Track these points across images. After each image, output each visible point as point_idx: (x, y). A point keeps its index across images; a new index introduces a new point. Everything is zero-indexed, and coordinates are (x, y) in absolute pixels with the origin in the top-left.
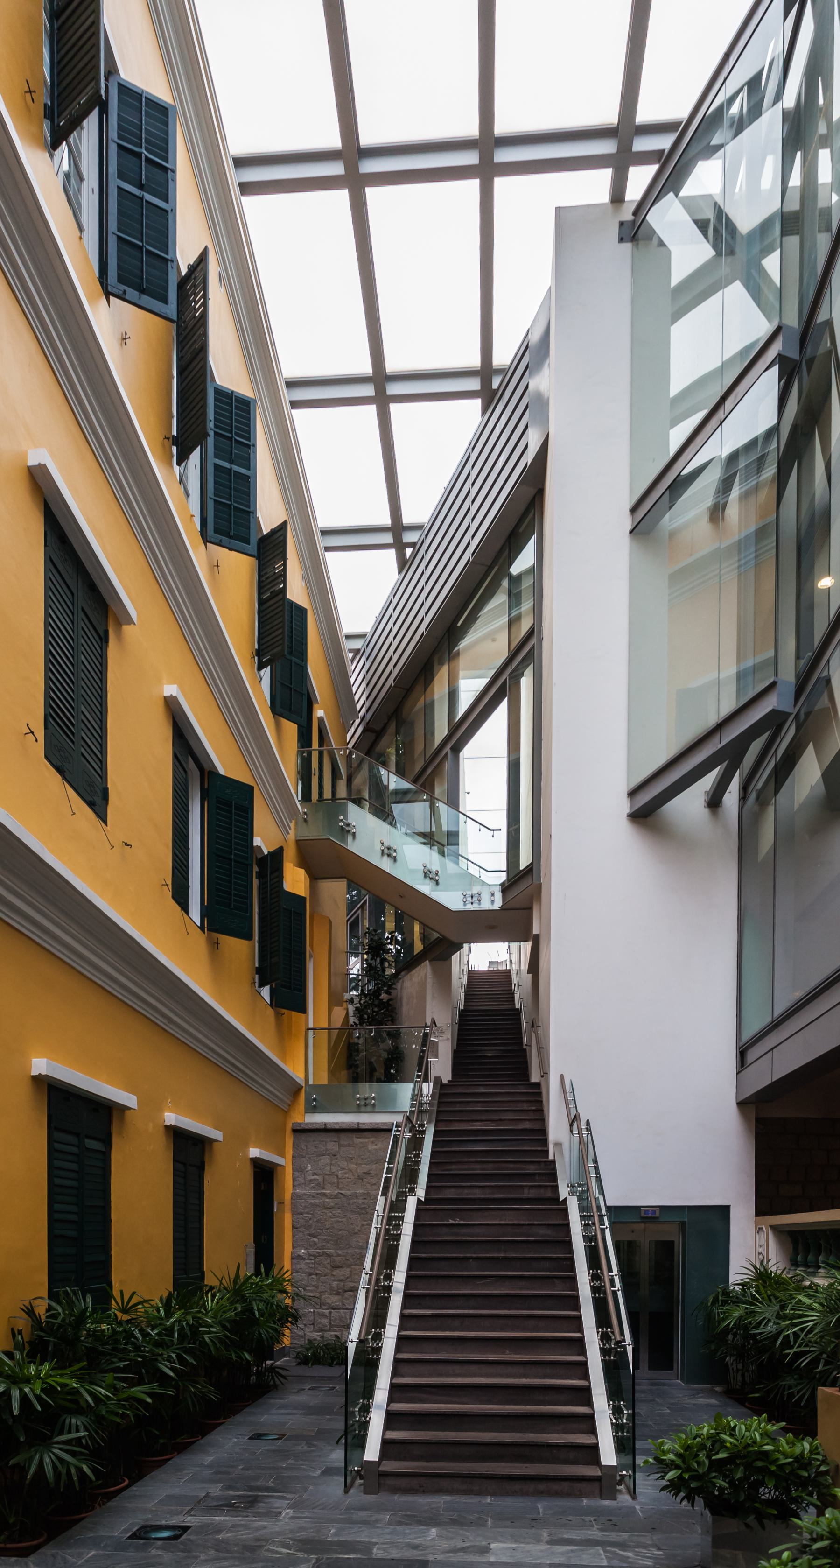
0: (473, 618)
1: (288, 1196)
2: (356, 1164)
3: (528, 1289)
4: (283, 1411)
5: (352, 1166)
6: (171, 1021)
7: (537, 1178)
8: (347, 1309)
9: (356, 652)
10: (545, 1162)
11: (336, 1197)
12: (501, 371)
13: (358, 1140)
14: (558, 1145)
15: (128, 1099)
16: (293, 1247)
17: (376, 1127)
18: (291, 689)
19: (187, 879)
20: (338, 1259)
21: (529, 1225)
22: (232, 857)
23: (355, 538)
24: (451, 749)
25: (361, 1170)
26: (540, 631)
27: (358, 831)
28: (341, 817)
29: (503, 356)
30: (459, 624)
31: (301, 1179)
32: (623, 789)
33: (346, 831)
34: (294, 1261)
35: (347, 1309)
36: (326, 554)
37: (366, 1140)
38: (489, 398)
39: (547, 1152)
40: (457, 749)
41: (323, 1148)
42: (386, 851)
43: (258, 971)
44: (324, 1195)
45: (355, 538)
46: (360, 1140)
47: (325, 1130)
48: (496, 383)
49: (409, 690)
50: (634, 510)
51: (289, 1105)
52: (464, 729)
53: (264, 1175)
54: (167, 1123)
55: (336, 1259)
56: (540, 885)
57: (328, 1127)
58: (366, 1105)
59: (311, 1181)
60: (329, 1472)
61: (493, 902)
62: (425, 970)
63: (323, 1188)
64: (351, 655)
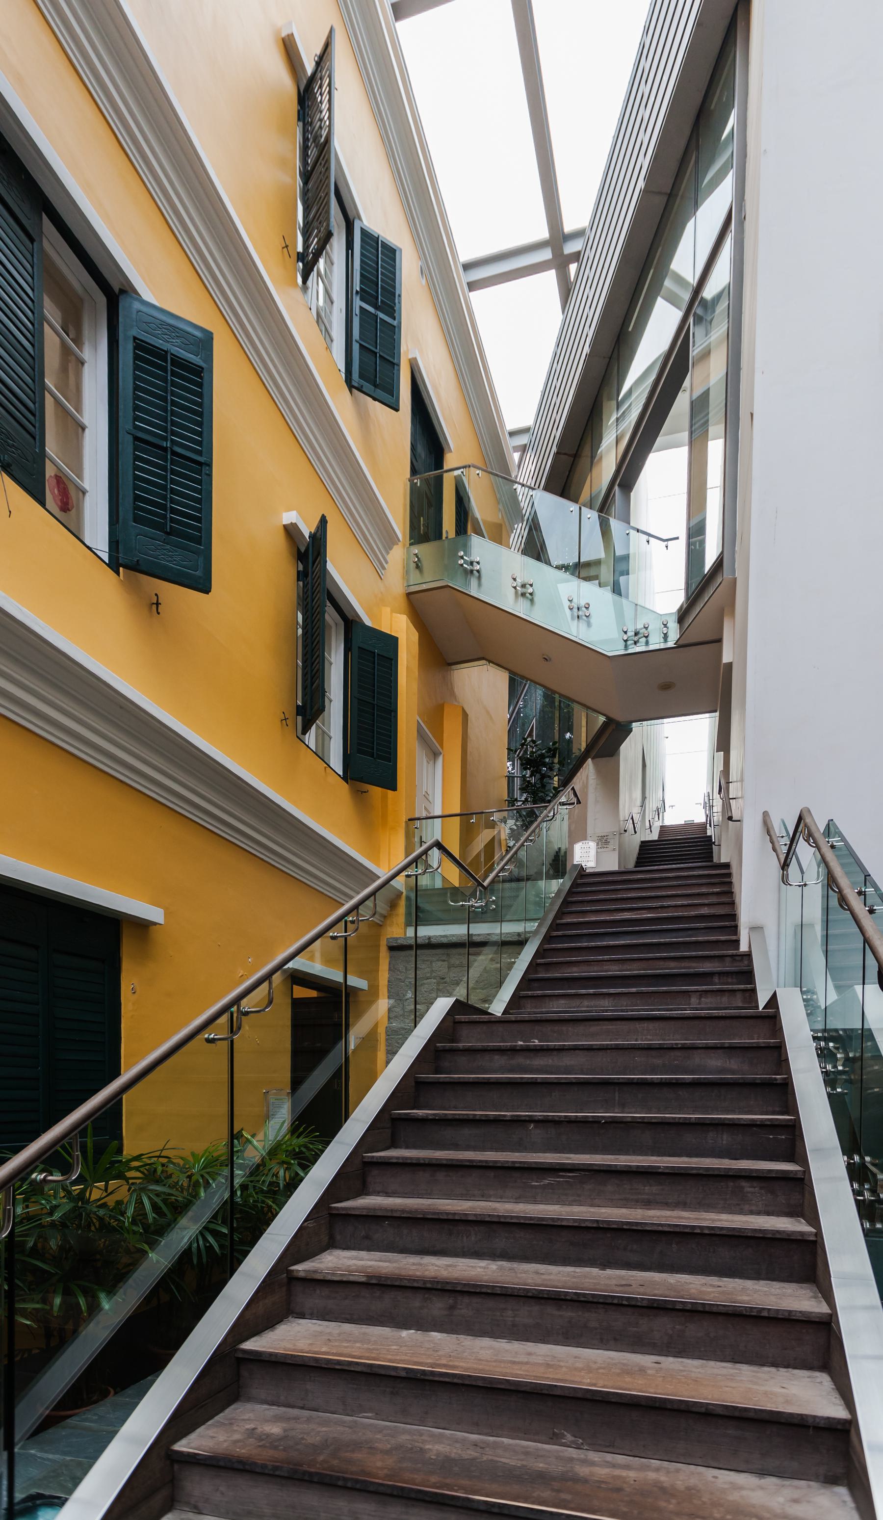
9: (524, 449)
10: (732, 956)
14: (756, 929)
21: (684, 1048)
23: (503, 267)
27: (485, 568)
28: (462, 553)
30: (630, 329)
33: (471, 572)
36: (472, 294)
39: (737, 942)
45: (503, 267)
49: (576, 456)
51: (385, 917)
56: (734, 581)
57: (433, 941)
61: (666, 637)
64: (516, 456)
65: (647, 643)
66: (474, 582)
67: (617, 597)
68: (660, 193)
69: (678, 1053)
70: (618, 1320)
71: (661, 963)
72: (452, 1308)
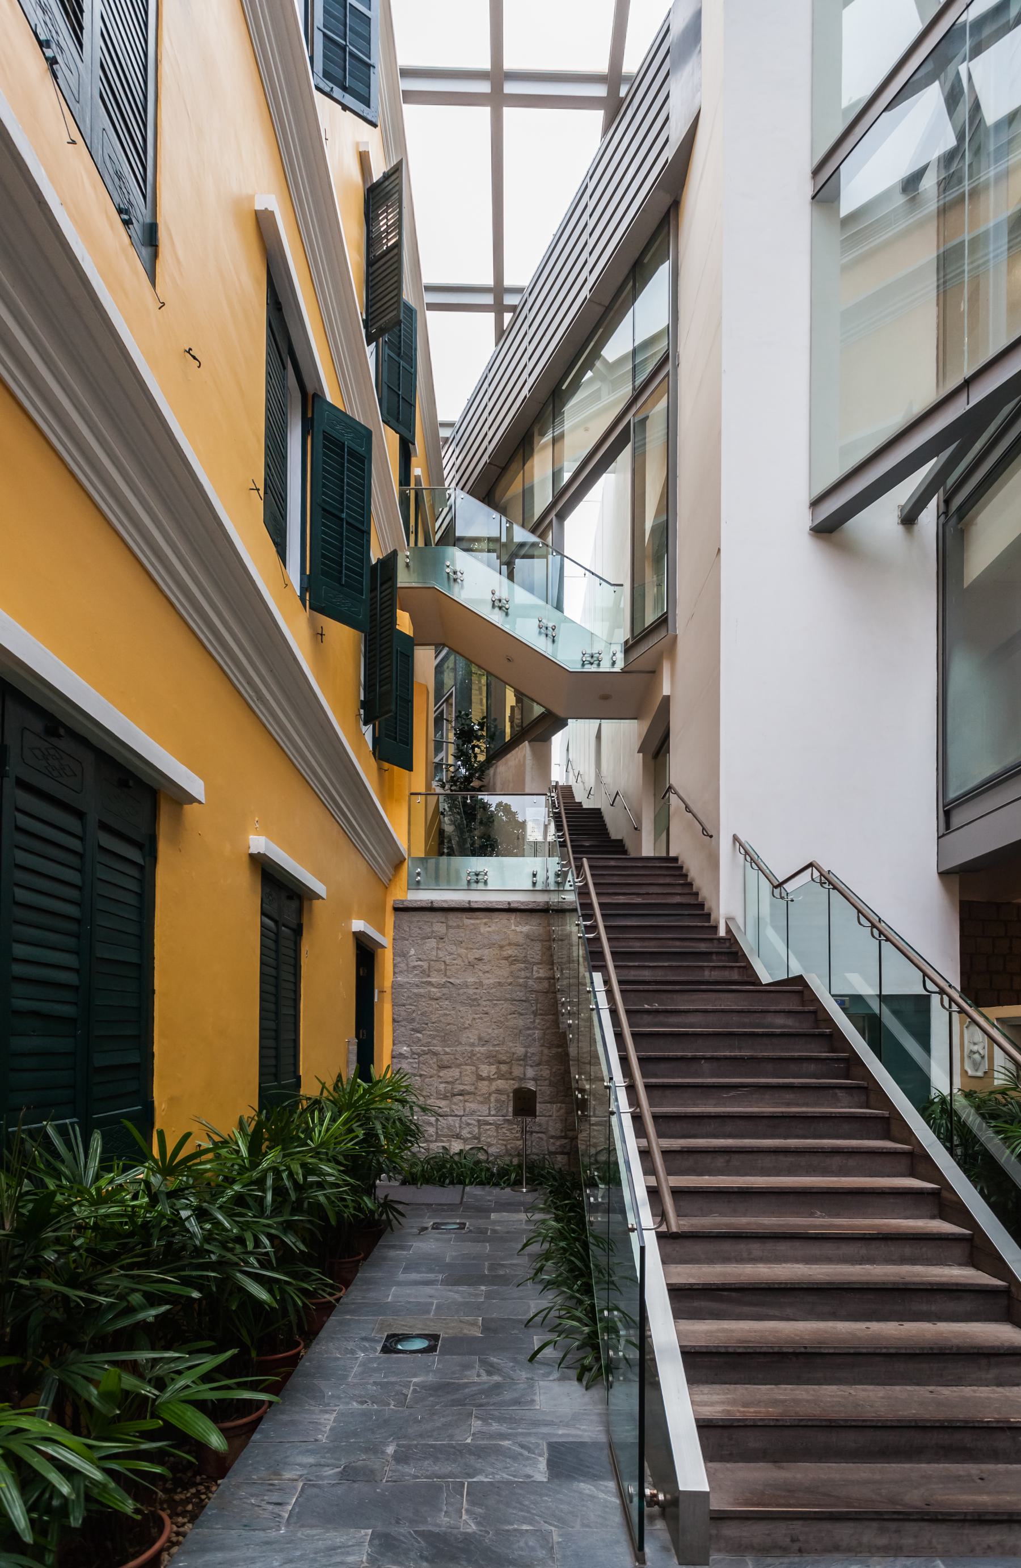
0: (575, 386)
1: (387, 984)
2: (467, 949)
3: (798, 1105)
4: (414, 1276)
5: (463, 951)
6: (261, 698)
7: (714, 957)
8: (456, 1116)
11: (443, 986)
12: (628, 79)
13: (468, 921)
15: (193, 784)
16: (394, 1044)
17: (490, 906)
18: (399, 395)
19: (284, 517)
20: (445, 1058)
21: (762, 1012)
22: (344, 516)
24: (556, 515)
25: (471, 957)
26: (676, 356)
28: (448, 563)
29: (631, 65)
31: (403, 966)
32: (804, 499)
33: (453, 579)
34: (395, 1060)
35: (456, 1116)
37: (478, 921)
38: (614, 109)
40: (562, 517)
41: (429, 930)
42: (497, 603)
43: (364, 705)
44: (430, 983)
46: (472, 921)
47: (431, 909)
48: (623, 92)
49: (504, 469)
50: (816, 172)
52: (568, 497)
53: (366, 953)
54: (254, 850)
55: (443, 1057)
56: (676, 636)
57: (435, 905)
58: (477, 882)
59: (414, 967)
60: (567, 1461)
61: (614, 663)
62: (525, 750)
63: (429, 976)
65: (599, 665)
66: (456, 588)
67: (511, 583)
68: (600, 304)
69: (758, 1015)
70: (815, 1160)
71: (670, 943)
72: (728, 1161)
